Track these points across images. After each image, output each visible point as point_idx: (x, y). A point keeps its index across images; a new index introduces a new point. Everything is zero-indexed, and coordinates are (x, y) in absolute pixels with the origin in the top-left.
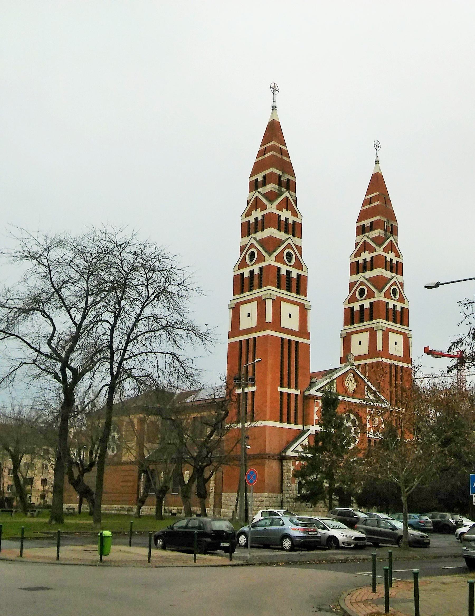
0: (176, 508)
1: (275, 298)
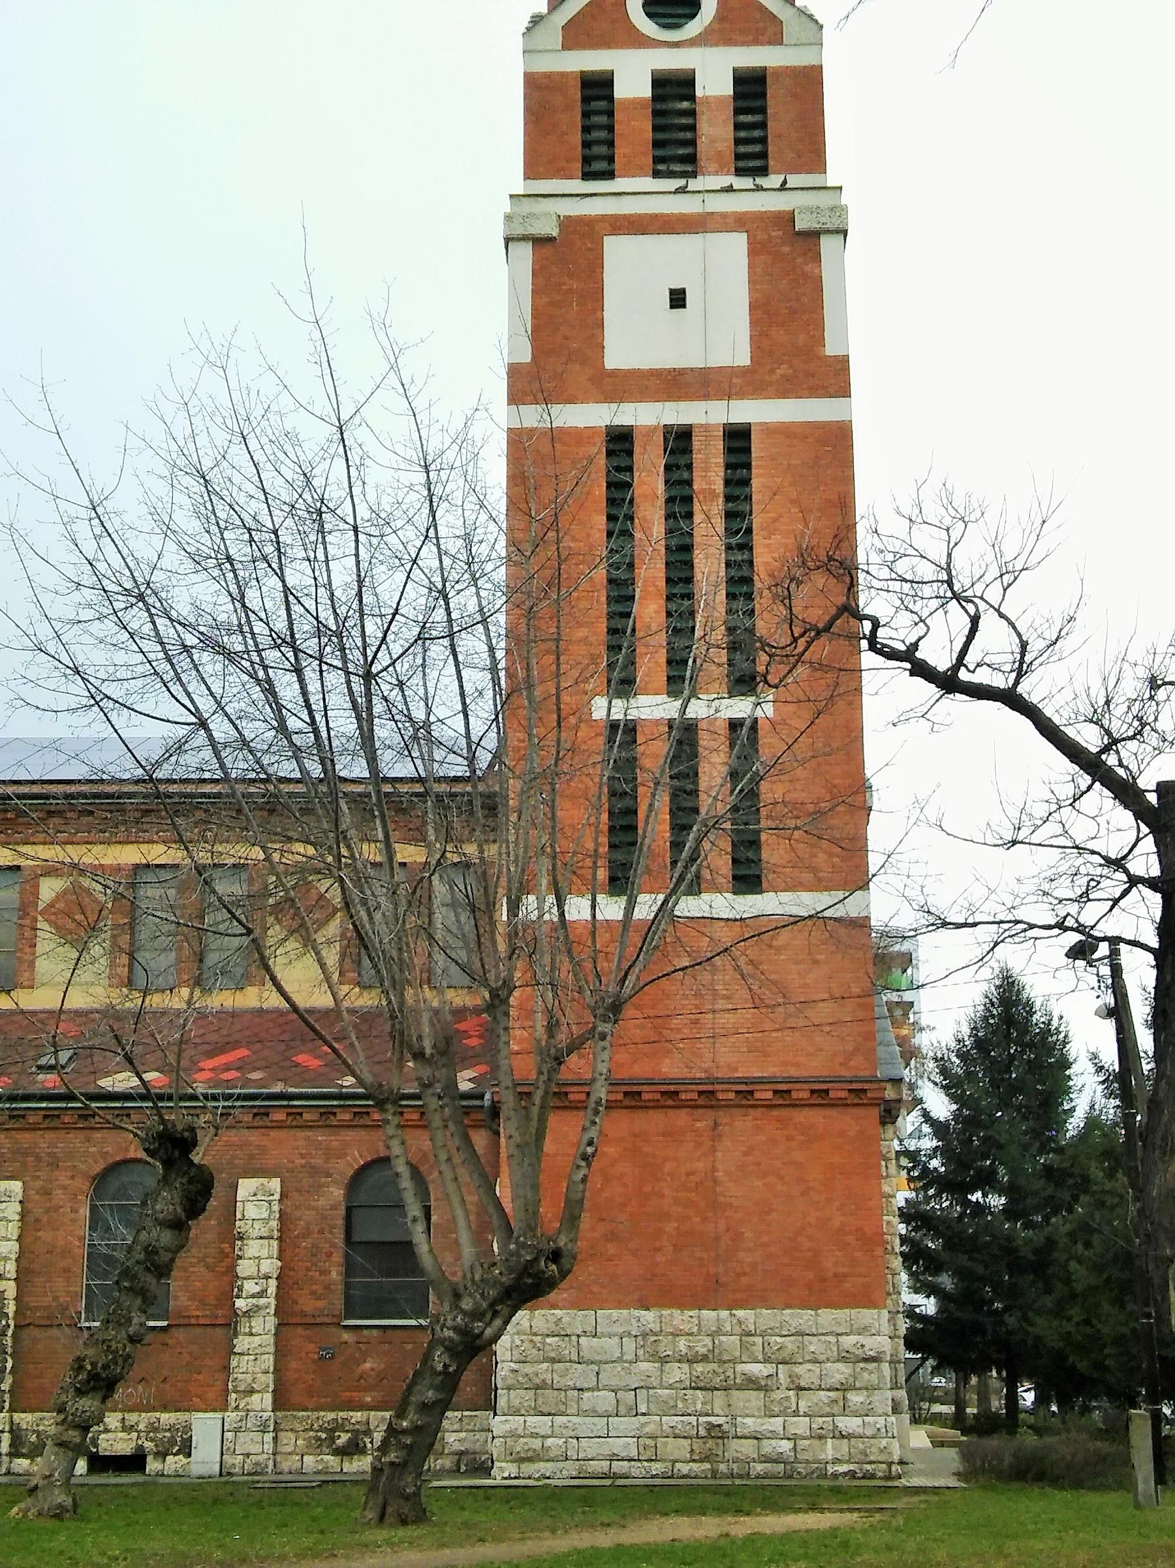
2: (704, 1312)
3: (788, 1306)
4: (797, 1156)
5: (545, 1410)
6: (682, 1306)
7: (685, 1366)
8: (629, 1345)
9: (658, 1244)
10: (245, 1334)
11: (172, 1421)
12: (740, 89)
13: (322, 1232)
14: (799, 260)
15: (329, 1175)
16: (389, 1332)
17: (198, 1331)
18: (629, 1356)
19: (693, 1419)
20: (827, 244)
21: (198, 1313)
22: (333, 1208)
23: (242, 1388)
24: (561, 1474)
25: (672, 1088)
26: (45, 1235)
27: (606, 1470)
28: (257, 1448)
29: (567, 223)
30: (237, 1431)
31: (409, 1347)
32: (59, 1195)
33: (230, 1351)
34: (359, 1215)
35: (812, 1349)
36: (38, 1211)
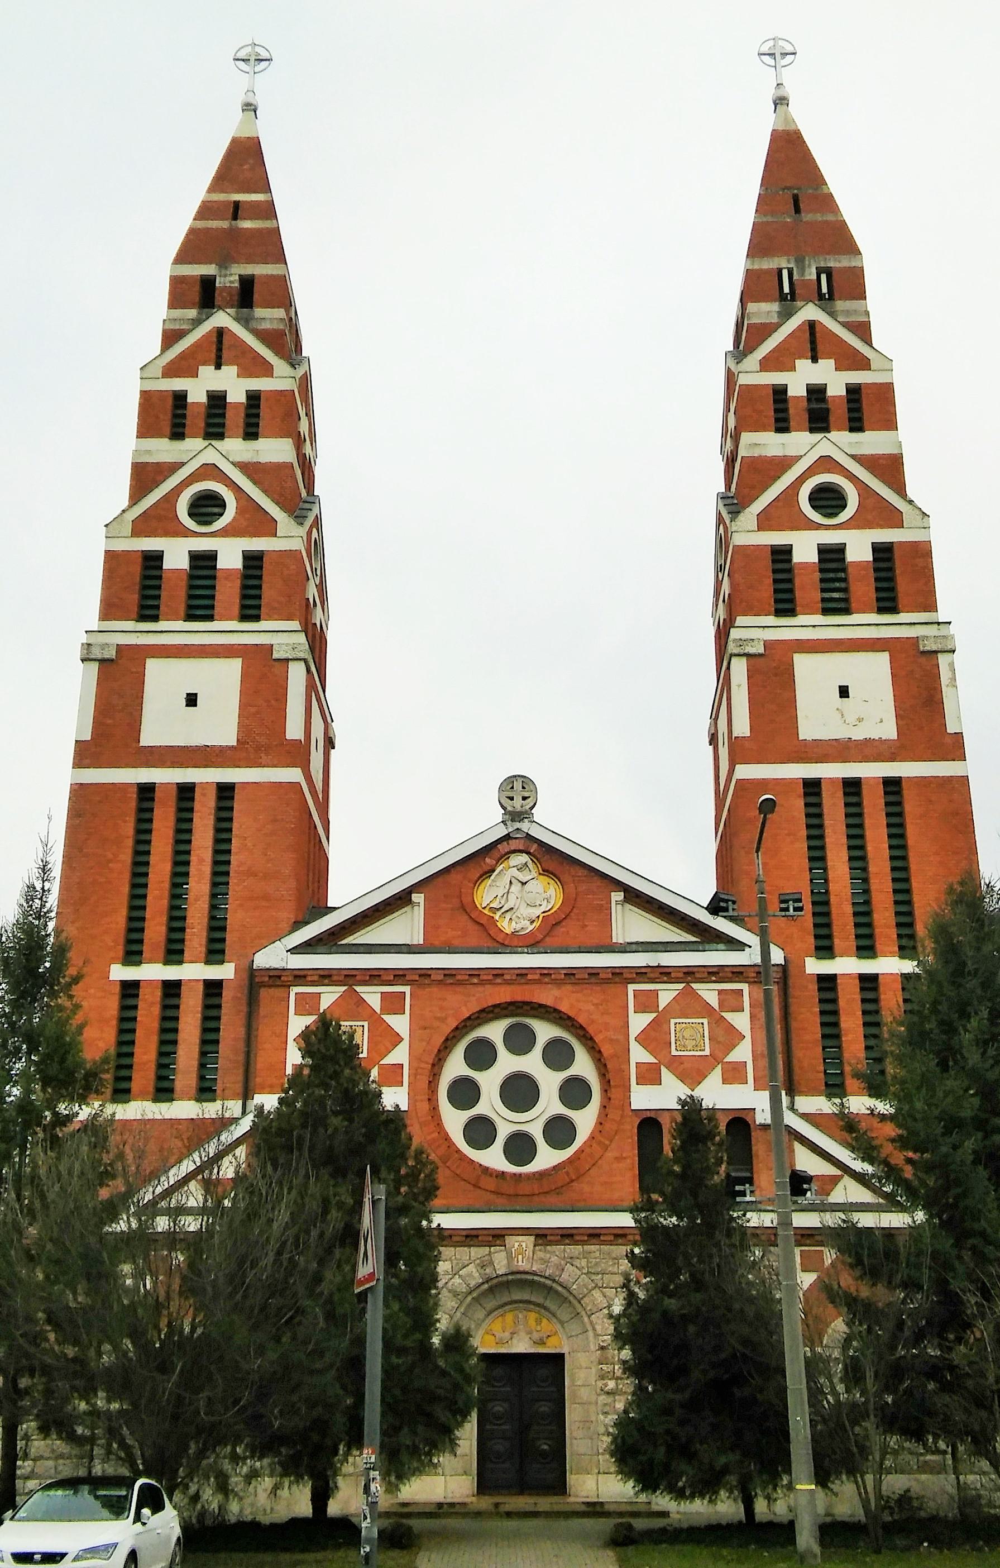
12: (822, 556)
20: (943, 660)
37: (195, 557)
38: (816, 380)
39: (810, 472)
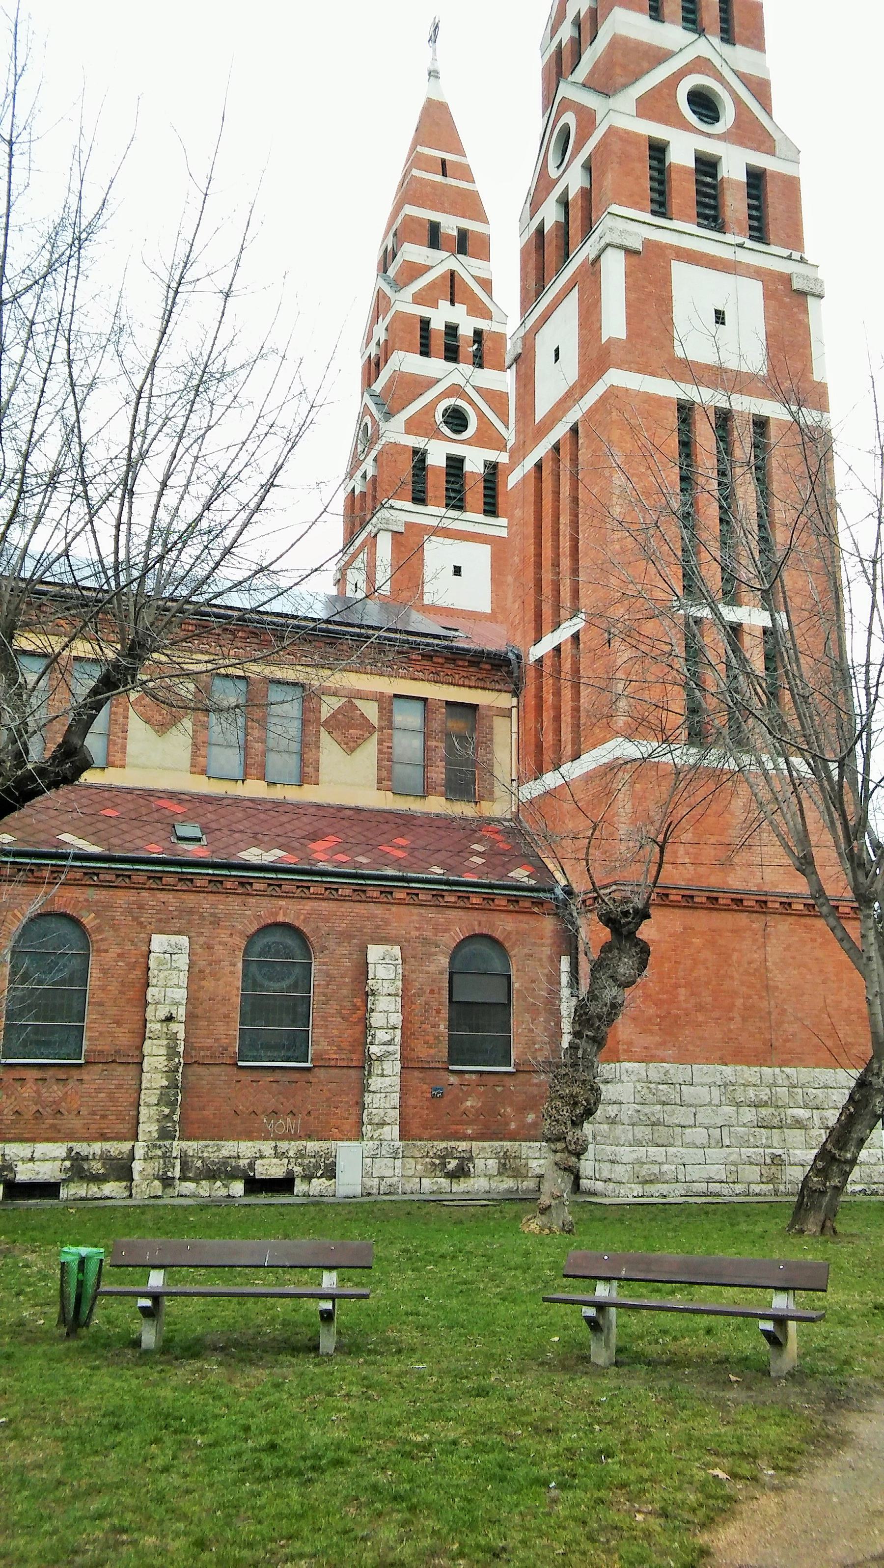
0: (59, 1150)
1: (402, 529)
2: (765, 1068)
3: (817, 1066)
4: (819, 953)
5: (660, 1142)
6: (749, 1064)
7: (753, 1109)
8: (716, 1092)
9: (731, 1015)
10: (378, 1075)
11: (317, 1149)
13: (432, 992)
14: (795, 310)
15: (437, 946)
16: (484, 1077)
17: (337, 1071)
18: (716, 1101)
19: (761, 1150)
21: (337, 1056)
22: (441, 973)
23: (376, 1121)
24: (675, 1193)
25: (739, 896)
26: (209, 984)
27: (705, 1190)
28: (390, 1173)
29: (647, 243)
30: (373, 1157)
31: (499, 1089)
32: (219, 950)
33: (364, 1088)
34: (455, 977)
35: (834, 1098)
36: (202, 963)
37: (450, 458)
38: (453, 320)
39: (446, 394)
